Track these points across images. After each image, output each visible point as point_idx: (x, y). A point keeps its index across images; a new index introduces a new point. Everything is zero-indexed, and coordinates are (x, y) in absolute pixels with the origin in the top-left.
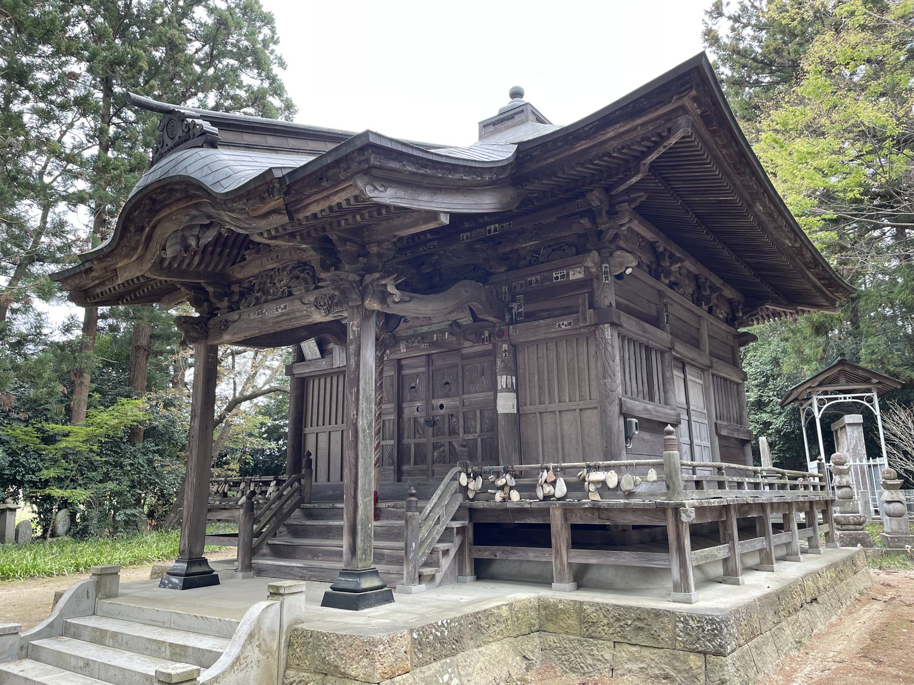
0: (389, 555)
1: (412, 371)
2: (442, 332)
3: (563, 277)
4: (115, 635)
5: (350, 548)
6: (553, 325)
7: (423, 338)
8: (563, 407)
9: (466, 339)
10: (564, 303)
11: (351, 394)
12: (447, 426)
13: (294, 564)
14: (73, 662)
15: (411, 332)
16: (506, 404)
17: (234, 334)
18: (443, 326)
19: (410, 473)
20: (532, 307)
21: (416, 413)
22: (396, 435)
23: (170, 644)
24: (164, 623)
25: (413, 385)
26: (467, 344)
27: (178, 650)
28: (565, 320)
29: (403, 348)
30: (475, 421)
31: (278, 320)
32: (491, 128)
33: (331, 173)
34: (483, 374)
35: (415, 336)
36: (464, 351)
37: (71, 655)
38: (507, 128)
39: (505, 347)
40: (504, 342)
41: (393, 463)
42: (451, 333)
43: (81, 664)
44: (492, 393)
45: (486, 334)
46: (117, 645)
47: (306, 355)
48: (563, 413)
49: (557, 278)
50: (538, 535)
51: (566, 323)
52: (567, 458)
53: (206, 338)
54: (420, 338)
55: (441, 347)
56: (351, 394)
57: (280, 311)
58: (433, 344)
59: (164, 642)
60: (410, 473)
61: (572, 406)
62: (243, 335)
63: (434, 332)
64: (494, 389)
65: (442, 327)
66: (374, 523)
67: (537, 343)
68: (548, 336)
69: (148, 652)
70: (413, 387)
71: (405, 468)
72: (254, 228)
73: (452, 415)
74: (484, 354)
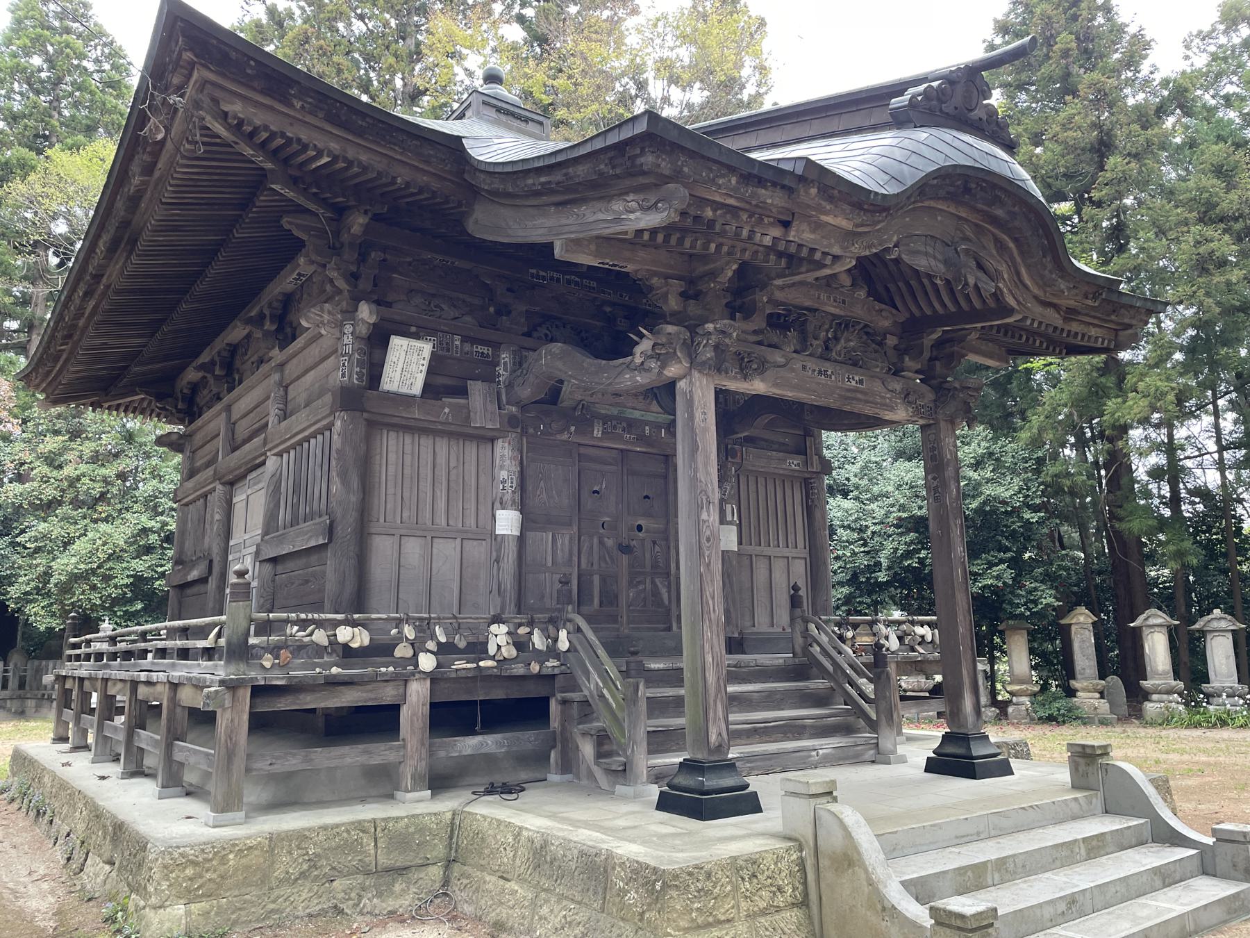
4: (1001, 863)
7: (630, 426)
12: (648, 555)
14: (1048, 912)
15: (615, 411)
21: (602, 531)
23: (1084, 839)
24: (978, 834)
25: (596, 488)
27: (1094, 843)
32: (492, 113)
35: (619, 419)
37: (1040, 905)
38: (509, 128)
43: (1062, 907)
46: (1007, 877)
47: (385, 378)
48: (435, 540)
50: (378, 721)
54: (624, 424)
57: (853, 383)
58: (641, 439)
59: (1076, 841)
63: (646, 423)
66: (682, 692)
69: (1058, 863)
70: (595, 492)
72: (1027, 308)
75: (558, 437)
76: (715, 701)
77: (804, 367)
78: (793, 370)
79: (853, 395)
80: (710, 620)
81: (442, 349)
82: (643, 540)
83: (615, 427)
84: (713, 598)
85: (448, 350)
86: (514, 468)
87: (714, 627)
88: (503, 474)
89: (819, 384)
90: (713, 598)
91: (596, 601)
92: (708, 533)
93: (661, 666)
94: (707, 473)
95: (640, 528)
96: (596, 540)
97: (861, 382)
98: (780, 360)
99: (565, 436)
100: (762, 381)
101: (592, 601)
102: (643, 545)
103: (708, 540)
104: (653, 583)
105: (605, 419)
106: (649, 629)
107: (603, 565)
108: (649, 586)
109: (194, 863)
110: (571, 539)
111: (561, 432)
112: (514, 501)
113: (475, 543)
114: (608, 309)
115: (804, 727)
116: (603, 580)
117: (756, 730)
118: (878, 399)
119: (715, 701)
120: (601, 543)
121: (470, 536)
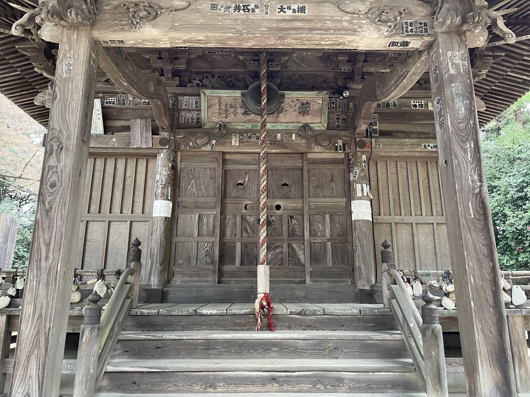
0: (352, 380)
1: (241, 167)
2: (289, 133)
3: (421, 106)
5: (498, 388)
6: (419, 145)
8: (420, 219)
9: (320, 145)
10: (420, 129)
11: (465, 151)
12: (285, 227)
16: (361, 211)
17: (174, 28)
18: (291, 126)
19: (233, 274)
20: (387, 127)
21: (244, 211)
22: (218, 231)
25: (240, 181)
26: (317, 149)
28: (430, 142)
29: (235, 142)
30: (324, 225)
31: (281, 25)
34: (332, 180)
36: (310, 156)
39: (364, 157)
40: (363, 153)
41: (213, 263)
42: (298, 135)
44: (344, 200)
45: (340, 143)
49: (415, 106)
51: (432, 145)
52: (423, 267)
53: (93, 25)
55: (285, 147)
56: (465, 151)
58: (274, 143)
60: (233, 274)
61: (430, 219)
62: (185, 36)
63: (278, 131)
64: (349, 195)
65: (290, 128)
67: (396, 159)
68: (411, 154)
71: (227, 268)
73: (292, 217)
74: (334, 162)
75: (203, 148)
76: (29, 357)
78: (198, 11)
79: (290, 25)
80: (39, 268)
81: (119, 104)
82: (281, 216)
83: (250, 137)
84: (48, 245)
85: (124, 104)
86: (164, 172)
87: (44, 276)
88: (158, 177)
89: (236, 20)
90: (48, 245)
91: (238, 261)
92: (54, 178)
93: (214, 312)
94: (64, 120)
95: (278, 207)
96: (238, 218)
97: (302, 10)
99: (208, 148)
100: (153, 27)
101: (234, 261)
102: (281, 220)
103: (53, 185)
104: (289, 246)
105: (241, 133)
106: (285, 282)
107: (245, 234)
108: (285, 249)
110: (214, 218)
111: (205, 145)
112: (163, 194)
113: (142, 224)
114: (241, 57)
115: (340, 380)
116: (244, 246)
117: (274, 379)
118: (329, 24)
119: (29, 357)
120: (243, 218)
121: (137, 219)
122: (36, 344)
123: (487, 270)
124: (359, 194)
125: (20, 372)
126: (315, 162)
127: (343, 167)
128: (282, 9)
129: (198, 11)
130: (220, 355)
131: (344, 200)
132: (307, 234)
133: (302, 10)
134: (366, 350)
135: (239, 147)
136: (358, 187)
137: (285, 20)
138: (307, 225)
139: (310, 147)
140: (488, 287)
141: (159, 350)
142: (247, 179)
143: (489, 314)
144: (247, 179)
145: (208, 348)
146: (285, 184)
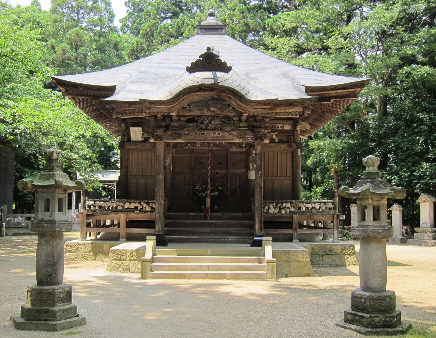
3: (281, 127)
13: (191, 237)
33: (295, 104)
44: (245, 170)
49: (278, 127)
64: (248, 169)
77: (196, 133)
78: (191, 135)
95: (217, 173)
97: (219, 134)
98: (186, 132)
109: (71, 246)
117: (212, 233)
118: (227, 138)
122: (160, 218)
123: (260, 203)
124: (251, 168)
125: (157, 224)
126: (233, 153)
127: (245, 155)
128: (214, 134)
129: (191, 135)
130: (169, 278)
131: (245, 170)
132: (229, 184)
133: (219, 134)
134: (242, 226)
135: (200, 147)
136: (251, 165)
137: (214, 137)
138: (229, 181)
139: (231, 147)
140: (260, 207)
141: (177, 225)
142: (204, 160)
143: (259, 213)
144: (204, 160)
145: (193, 225)
146: (220, 163)
